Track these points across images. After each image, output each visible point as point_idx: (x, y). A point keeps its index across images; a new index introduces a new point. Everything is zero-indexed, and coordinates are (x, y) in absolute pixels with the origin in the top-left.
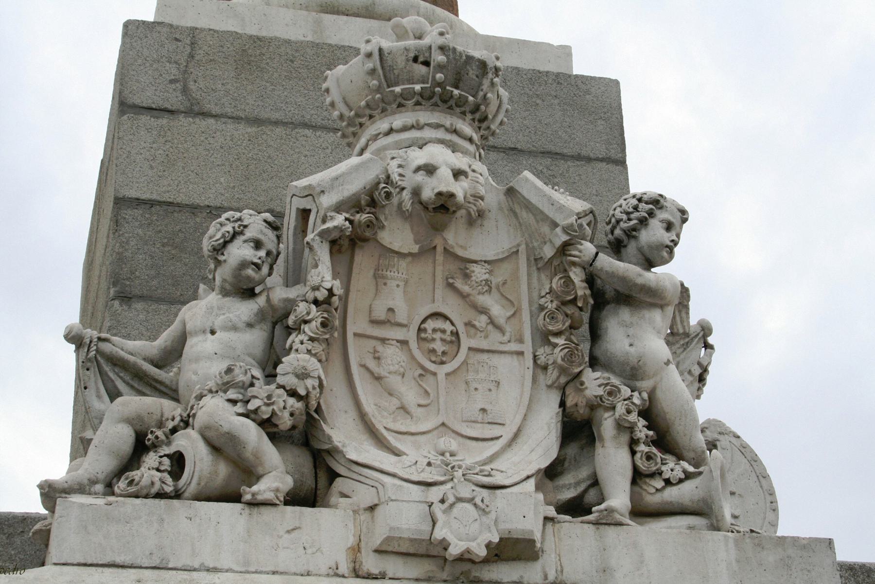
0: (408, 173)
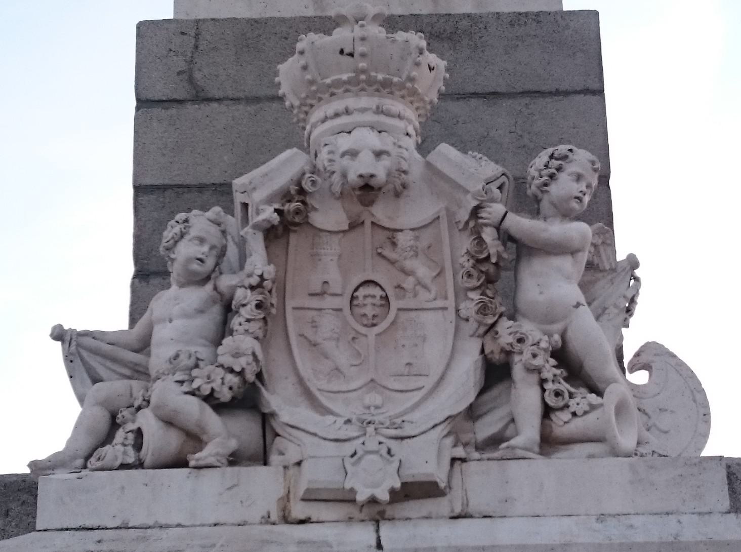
0: (337, 157)
